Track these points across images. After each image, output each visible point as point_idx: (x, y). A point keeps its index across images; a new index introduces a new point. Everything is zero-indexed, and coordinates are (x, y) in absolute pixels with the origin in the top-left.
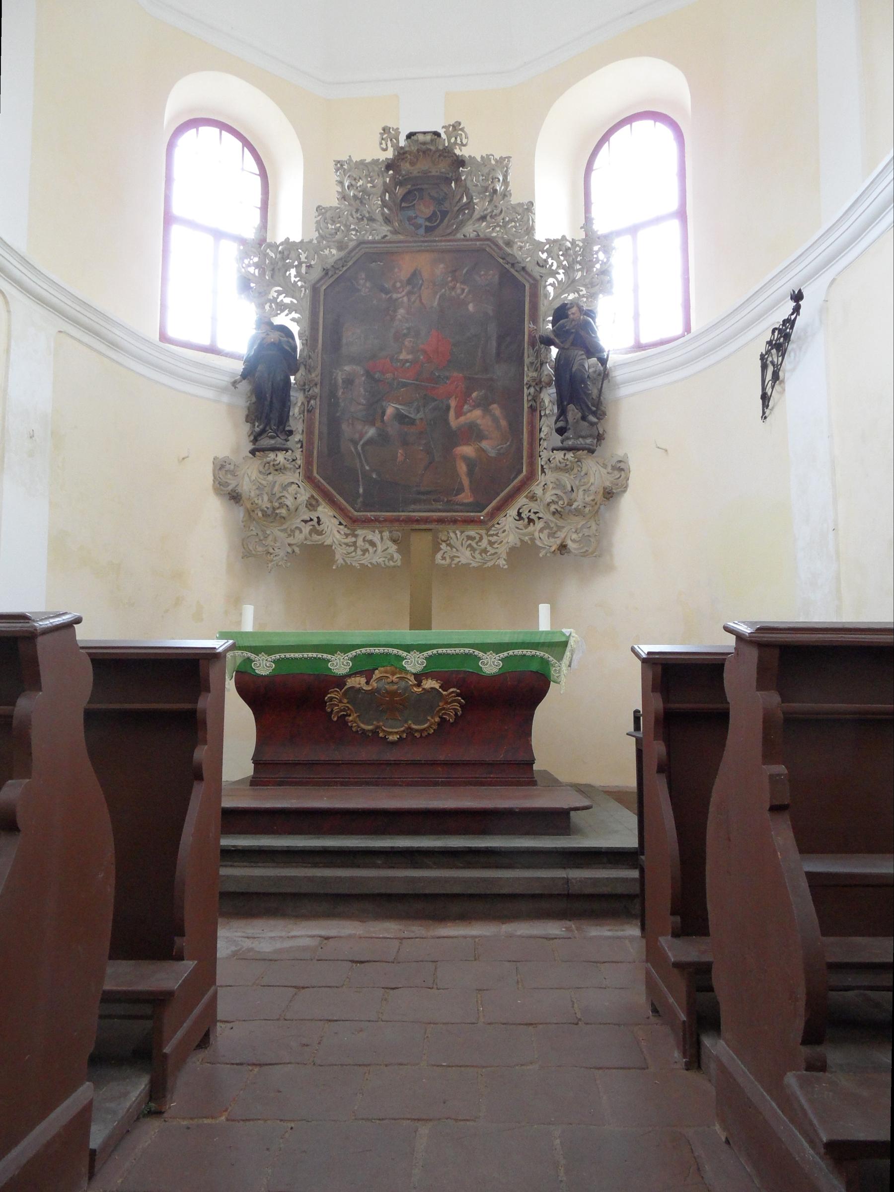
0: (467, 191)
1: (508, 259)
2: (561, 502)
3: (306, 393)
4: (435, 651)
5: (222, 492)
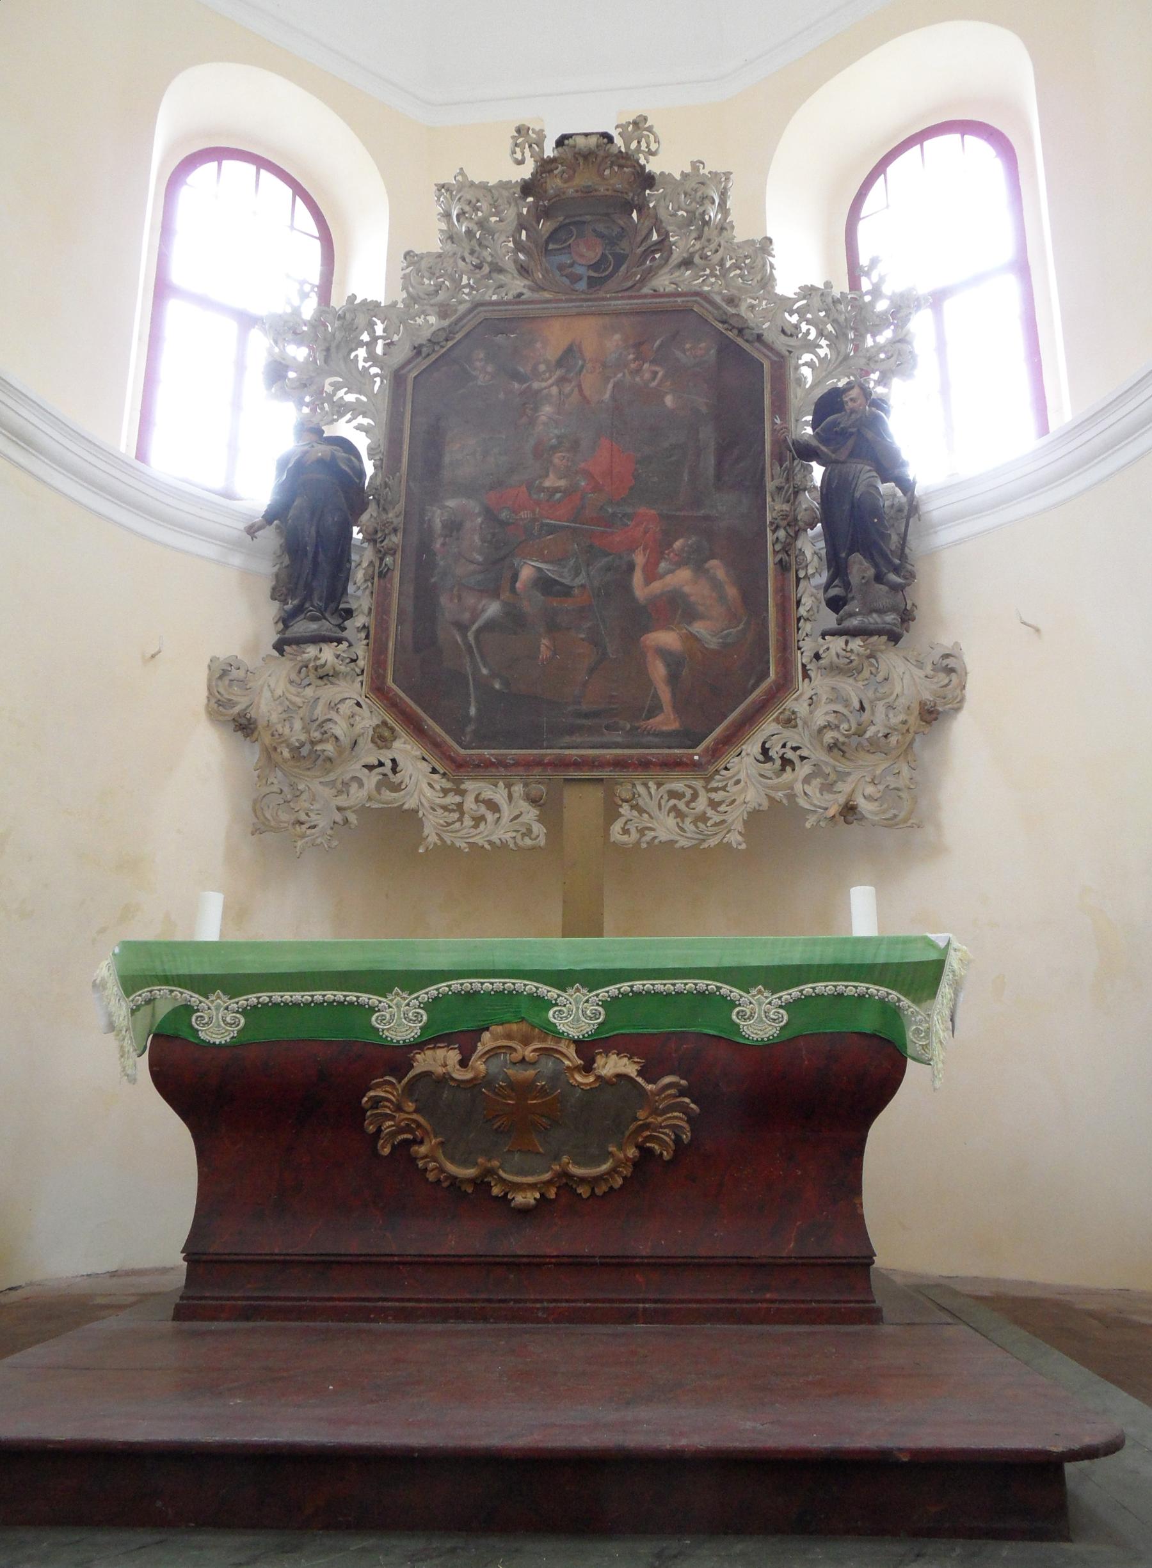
0: (657, 224)
1: (733, 321)
2: (844, 726)
3: (378, 545)
4: (625, 987)
5: (221, 718)
